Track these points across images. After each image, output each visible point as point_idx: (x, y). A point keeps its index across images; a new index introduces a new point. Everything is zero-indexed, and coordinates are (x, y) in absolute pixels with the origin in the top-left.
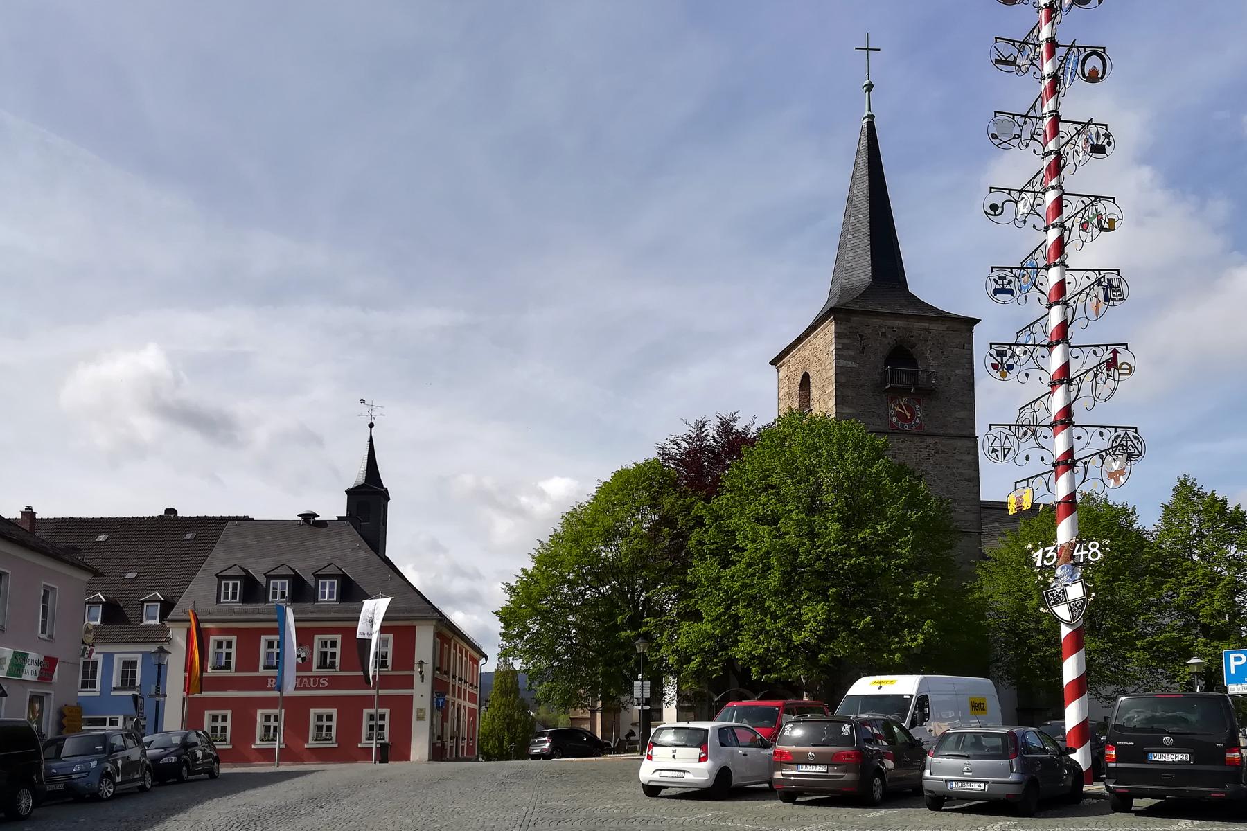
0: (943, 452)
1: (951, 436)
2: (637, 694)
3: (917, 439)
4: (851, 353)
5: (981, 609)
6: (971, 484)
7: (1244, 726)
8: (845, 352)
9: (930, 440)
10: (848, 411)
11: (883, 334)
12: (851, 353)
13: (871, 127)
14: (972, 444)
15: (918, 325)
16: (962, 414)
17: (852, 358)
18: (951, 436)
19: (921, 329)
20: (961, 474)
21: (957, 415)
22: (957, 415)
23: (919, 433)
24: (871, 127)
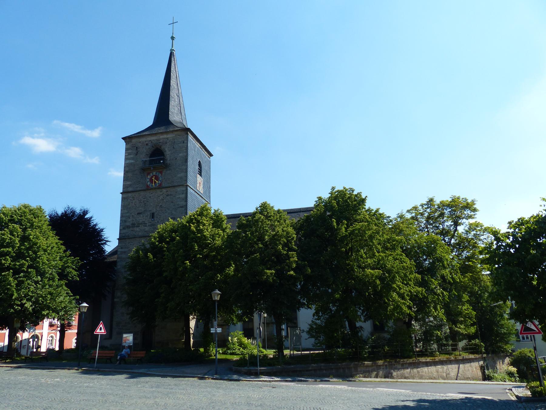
0: (171, 195)
1: (174, 187)
2: (218, 329)
3: (158, 191)
4: (132, 156)
5: (104, 251)
6: (183, 209)
7: (544, 374)
8: (129, 157)
9: (164, 190)
10: (129, 183)
11: (147, 144)
12: (132, 156)
13: (171, 54)
14: (184, 189)
15: (162, 137)
16: (182, 175)
17: (132, 159)
18: (174, 187)
19: (164, 139)
20: (178, 205)
21: (179, 175)
22: (179, 175)
23: (160, 187)
24: (171, 54)
